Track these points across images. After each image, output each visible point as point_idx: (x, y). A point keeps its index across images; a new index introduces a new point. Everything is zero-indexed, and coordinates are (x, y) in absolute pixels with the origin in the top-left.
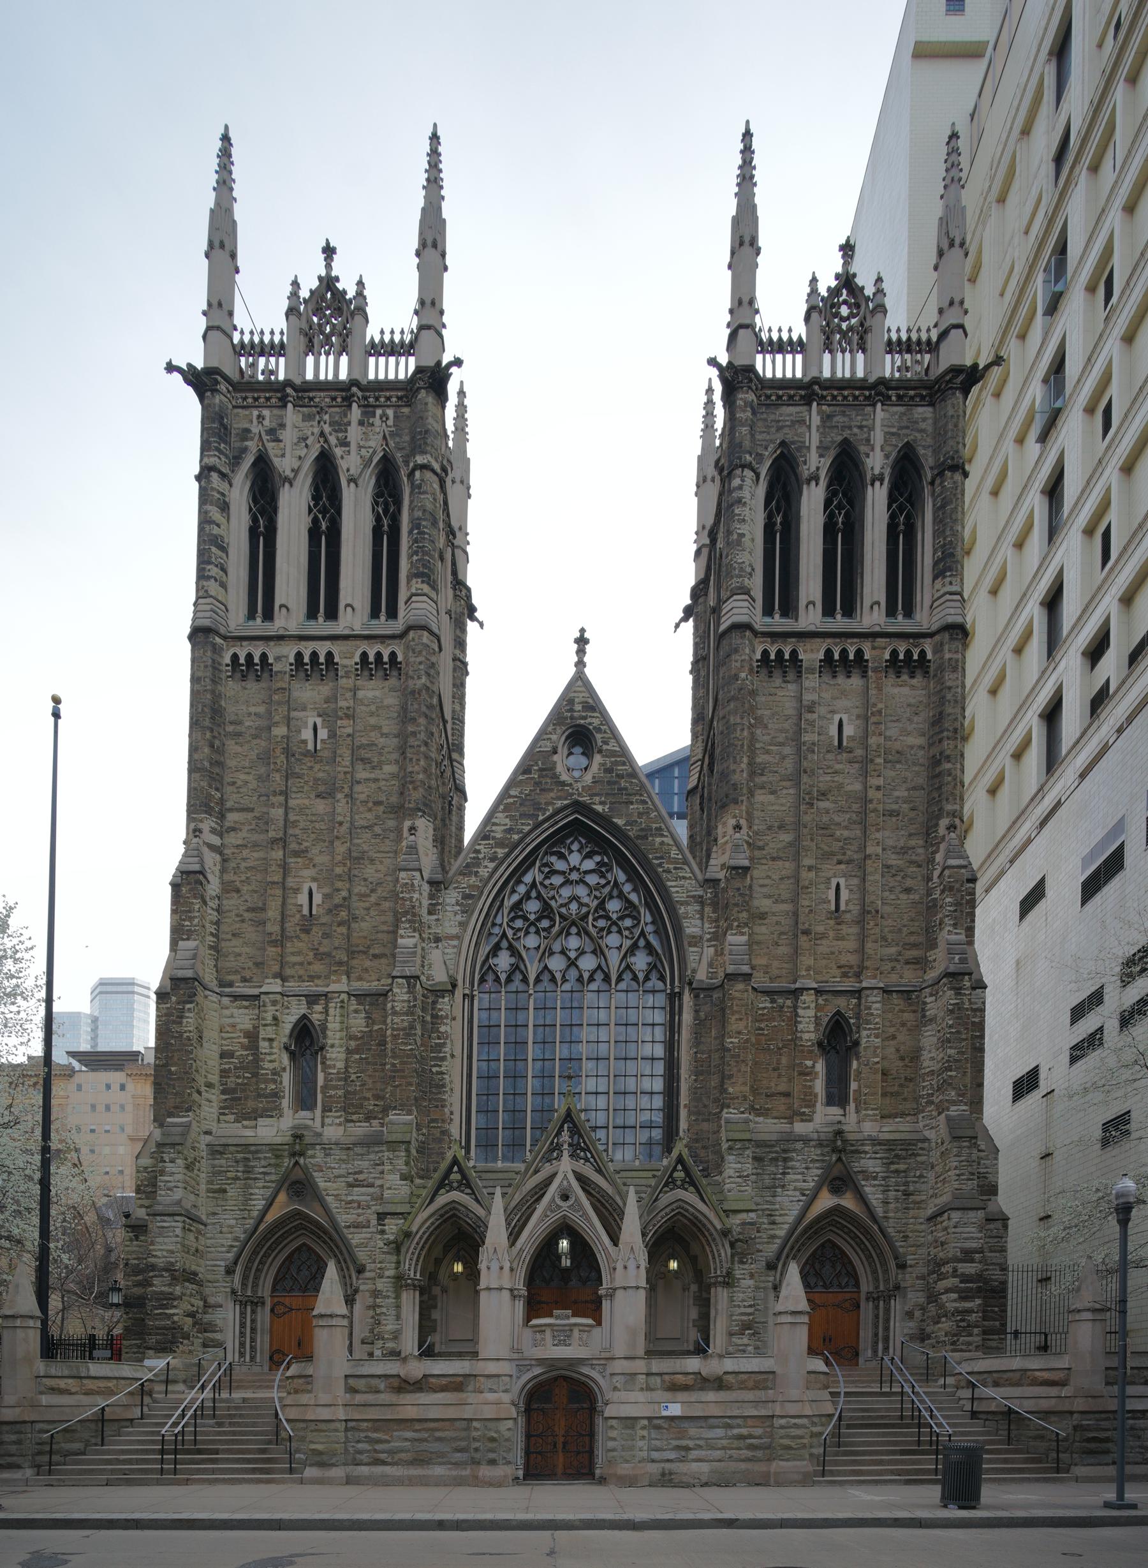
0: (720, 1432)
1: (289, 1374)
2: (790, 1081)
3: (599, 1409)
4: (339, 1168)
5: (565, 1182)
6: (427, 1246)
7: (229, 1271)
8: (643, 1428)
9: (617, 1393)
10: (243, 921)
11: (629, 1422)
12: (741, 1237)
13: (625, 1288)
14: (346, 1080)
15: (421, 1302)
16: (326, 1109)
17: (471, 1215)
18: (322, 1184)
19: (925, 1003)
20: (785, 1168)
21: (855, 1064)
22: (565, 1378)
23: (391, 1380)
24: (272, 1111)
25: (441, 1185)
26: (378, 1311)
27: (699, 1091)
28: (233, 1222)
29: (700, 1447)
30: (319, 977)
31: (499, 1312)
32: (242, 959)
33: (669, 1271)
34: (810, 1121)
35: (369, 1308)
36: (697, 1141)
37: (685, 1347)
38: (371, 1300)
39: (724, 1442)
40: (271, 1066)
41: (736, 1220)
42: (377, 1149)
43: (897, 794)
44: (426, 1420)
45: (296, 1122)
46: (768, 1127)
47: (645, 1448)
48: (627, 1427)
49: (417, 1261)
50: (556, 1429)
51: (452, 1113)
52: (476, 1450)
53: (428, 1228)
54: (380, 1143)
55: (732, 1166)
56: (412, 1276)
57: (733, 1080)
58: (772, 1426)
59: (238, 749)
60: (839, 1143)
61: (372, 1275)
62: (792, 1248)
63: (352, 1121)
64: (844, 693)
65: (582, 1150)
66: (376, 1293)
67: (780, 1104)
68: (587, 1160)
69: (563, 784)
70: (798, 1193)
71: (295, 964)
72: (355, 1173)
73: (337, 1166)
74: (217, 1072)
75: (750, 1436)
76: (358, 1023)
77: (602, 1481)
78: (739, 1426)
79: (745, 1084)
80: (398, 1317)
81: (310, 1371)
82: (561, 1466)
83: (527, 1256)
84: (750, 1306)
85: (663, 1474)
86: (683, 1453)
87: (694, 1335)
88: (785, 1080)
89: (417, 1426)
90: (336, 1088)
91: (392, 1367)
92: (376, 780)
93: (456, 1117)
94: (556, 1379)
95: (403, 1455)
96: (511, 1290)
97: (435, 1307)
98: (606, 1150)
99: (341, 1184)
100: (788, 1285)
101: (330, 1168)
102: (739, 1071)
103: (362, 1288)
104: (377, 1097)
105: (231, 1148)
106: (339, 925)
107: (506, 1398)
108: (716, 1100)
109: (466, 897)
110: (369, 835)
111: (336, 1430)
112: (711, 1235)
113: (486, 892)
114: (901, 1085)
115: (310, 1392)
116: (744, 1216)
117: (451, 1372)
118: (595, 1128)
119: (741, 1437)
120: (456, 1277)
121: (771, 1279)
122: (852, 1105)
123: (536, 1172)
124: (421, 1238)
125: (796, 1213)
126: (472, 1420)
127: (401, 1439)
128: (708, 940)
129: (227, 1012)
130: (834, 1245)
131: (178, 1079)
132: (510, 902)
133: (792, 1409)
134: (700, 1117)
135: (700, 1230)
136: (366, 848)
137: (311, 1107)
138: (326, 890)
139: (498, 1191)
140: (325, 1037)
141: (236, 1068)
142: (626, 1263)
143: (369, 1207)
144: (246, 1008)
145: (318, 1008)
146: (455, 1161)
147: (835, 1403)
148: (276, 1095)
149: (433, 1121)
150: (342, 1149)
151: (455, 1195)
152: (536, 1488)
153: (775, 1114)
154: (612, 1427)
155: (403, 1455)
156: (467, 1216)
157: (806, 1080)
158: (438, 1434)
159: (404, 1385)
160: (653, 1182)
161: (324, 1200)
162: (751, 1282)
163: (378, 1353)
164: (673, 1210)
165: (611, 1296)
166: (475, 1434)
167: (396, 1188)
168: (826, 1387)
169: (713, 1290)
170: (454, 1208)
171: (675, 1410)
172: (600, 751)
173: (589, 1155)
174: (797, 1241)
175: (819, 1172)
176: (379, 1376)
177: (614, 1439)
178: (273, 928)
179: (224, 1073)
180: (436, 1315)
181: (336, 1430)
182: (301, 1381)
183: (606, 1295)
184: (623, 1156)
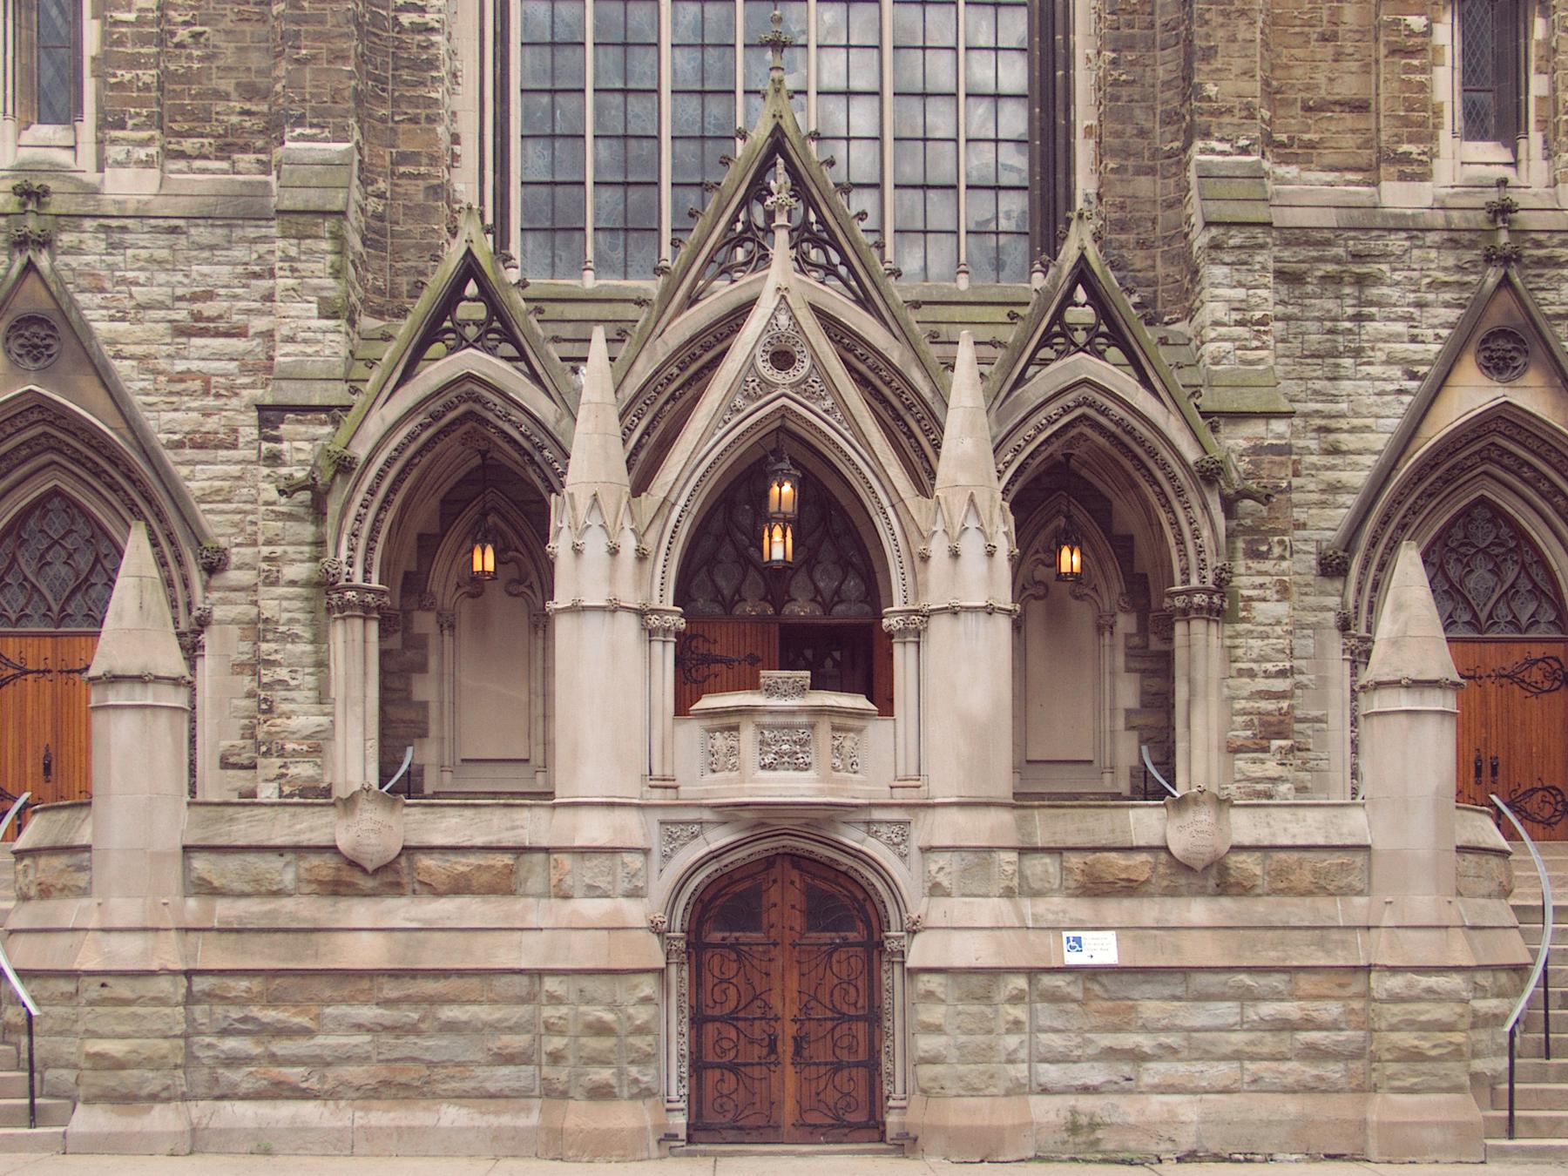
0: (1226, 1011)
1: (23, 842)
2: (1366, 70)
3: (890, 945)
4: (150, 282)
5: (783, 319)
6: (398, 499)
8: (1016, 999)
9: (941, 903)
11: (975, 980)
12: (1252, 484)
13: (954, 611)
14: (161, 42)
15: (384, 654)
16: (109, 122)
17: (517, 415)
18: (102, 328)
20: (1362, 303)
21: (1539, 28)
22: (798, 860)
23: (315, 860)
25: (432, 333)
26: (267, 675)
27: (1125, 92)
29: (1171, 1052)
31: (606, 668)
33: (1060, 577)
34: (1424, 177)
35: (239, 668)
36: (1122, 226)
37: (1107, 784)
38: (246, 646)
39: (1238, 1039)
41: (1235, 440)
42: (251, 232)
44: (414, 974)
45: (25, 154)
46: (1309, 194)
47: (1023, 1054)
48: (973, 997)
49: (372, 538)
50: (776, 1002)
51: (456, 139)
52: (556, 1058)
53: (400, 449)
54: (261, 217)
55: (1220, 290)
56: (358, 580)
57: (1218, 63)
58: (1367, 995)
60: (1503, 238)
61: (247, 577)
62: (1385, 521)
65: (818, 243)
66: (259, 628)
67: (1342, 131)
68: (830, 270)
70: (1396, 372)
72: (194, 298)
73: (142, 277)
75: (1309, 1024)
77: (906, 1145)
78: (1279, 997)
79: (1248, 73)
80: (322, 696)
81: (84, 836)
82: (789, 1106)
83: (681, 519)
84: (1282, 673)
85: (1074, 1128)
86: (1127, 1069)
87: (1128, 751)
88: (1354, 66)
89: (390, 990)
90: (134, 62)
91: (313, 826)
93: (468, 150)
94: (769, 861)
95: (353, 1073)
96: (642, 613)
97: (422, 668)
98: (880, 246)
99: (154, 326)
100: (1399, 607)
101: (123, 281)
102: (1232, 39)
103: (217, 613)
104: (250, 91)
107: (636, 912)
108: (1170, 118)
111: (160, 1001)
112: (1172, 478)
115: (84, 892)
116: (1257, 428)
117: (479, 841)
118: (846, 188)
119: (1284, 1026)
120: (477, 584)
121: (1334, 601)
122: (1535, 138)
123: (692, 300)
124: (380, 476)
125: (1393, 424)
126: (540, 973)
127: (343, 1029)
130: (1498, 515)
133: (1422, 949)
134: (1131, 163)
135: (1141, 465)
137: (69, 114)
139: (598, 348)
142: (954, 550)
143: (233, 391)
146: (470, 268)
147: (1530, 937)
149: (404, 158)
150: (155, 230)
151: (472, 360)
152: (724, 1162)
153: (1330, 158)
154: (929, 995)
155: (353, 1073)
156: (506, 417)
157: (1409, 69)
158: (449, 1013)
159: (350, 876)
160: (1009, 334)
161: (107, 367)
162: (1281, 609)
163: (268, 792)
164: (1066, 410)
165: (918, 636)
166: (549, 1012)
167: (311, 341)
168: (1506, 893)
169: (1180, 628)
170: (478, 399)
171: (1101, 949)
173: (835, 258)
174: (1397, 501)
175: (1453, 315)
176: (279, 850)
177: (937, 1029)
180: (425, 689)
181: (160, 1001)
182: (60, 862)
183: (904, 632)
184: (916, 267)
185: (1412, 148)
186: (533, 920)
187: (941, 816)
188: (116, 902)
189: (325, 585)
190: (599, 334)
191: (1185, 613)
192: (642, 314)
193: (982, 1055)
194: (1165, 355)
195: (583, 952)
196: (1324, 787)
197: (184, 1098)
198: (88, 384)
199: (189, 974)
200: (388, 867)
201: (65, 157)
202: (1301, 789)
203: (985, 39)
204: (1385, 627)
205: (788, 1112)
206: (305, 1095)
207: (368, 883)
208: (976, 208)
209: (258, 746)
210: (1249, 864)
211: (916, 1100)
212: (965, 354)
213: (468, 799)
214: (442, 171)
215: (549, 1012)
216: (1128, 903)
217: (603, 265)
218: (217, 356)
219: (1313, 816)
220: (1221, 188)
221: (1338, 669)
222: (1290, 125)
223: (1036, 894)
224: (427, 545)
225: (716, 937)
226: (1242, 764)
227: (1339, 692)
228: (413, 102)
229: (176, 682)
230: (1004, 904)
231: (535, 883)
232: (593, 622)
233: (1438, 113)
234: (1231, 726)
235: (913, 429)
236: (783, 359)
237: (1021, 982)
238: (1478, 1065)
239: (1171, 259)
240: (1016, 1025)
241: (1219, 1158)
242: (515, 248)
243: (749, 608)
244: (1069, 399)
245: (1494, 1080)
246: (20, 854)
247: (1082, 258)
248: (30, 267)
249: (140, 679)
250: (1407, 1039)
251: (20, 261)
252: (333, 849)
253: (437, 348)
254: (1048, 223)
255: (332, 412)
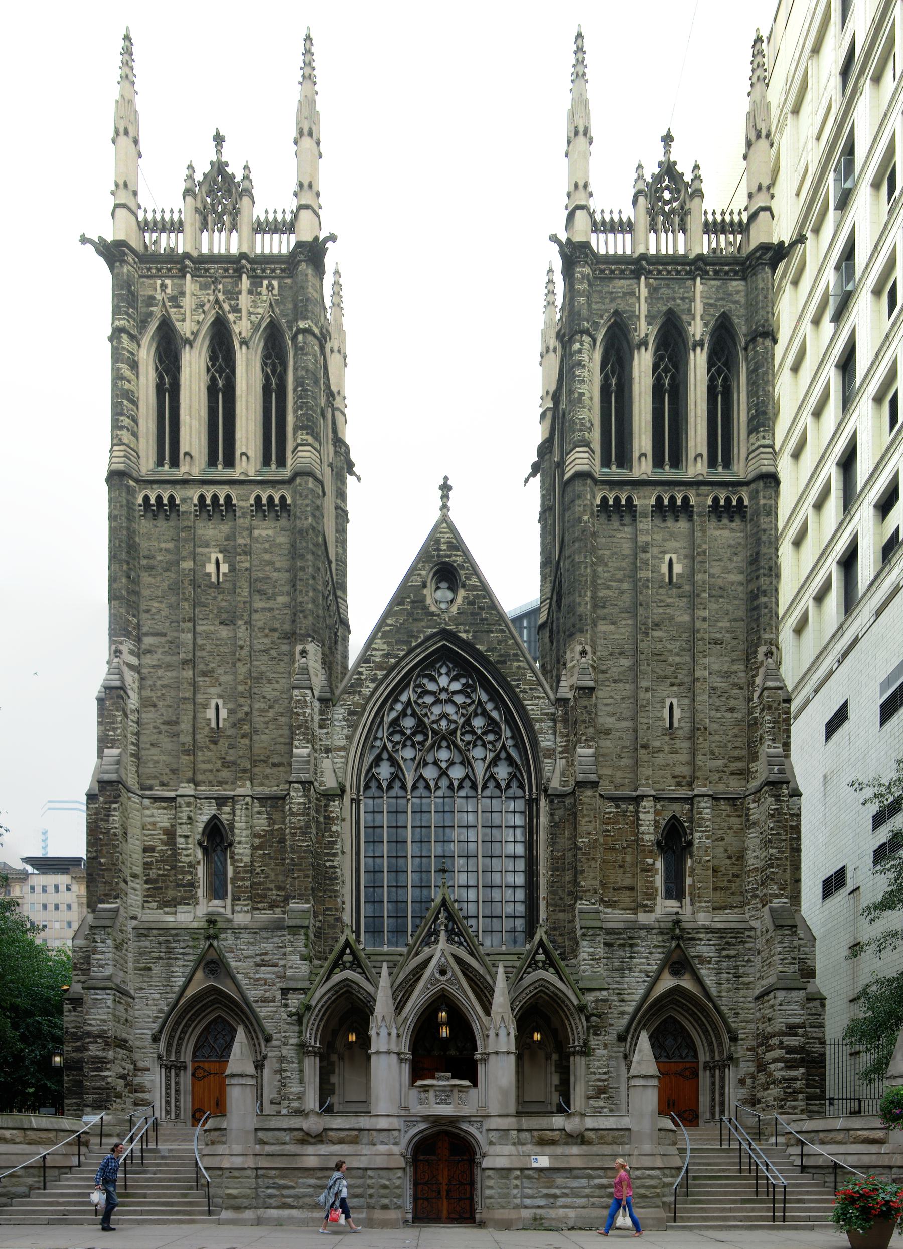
0: (584, 1182)
1: (206, 1127)
5: (443, 959)
7: (155, 1039)
8: (517, 1178)
9: (493, 1147)
10: (160, 733)
13: (497, 1053)
14: (252, 873)
15: (321, 1068)
16: (236, 898)
17: (362, 991)
18: (233, 964)
19: (749, 809)
21: (689, 863)
22: (447, 1133)
23: (296, 1133)
24: (189, 899)
26: (284, 1074)
28: (157, 996)
29: (566, 1195)
30: (226, 783)
31: (387, 1072)
32: (160, 765)
34: (652, 912)
35: (276, 1072)
36: (555, 929)
37: (549, 1109)
39: (588, 1191)
40: (187, 860)
41: (590, 997)
43: (720, 624)
46: (615, 917)
49: (317, 1031)
51: (343, 903)
52: (371, 1196)
53: (326, 1002)
54: (282, 928)
55: (586, 950)
59: (150, 580)
60: (677, 931)
62: (638, 1024)
63: (258, 909)
64: (673, 535)
65: (456, 934)
66: (282, 1059)
67: (625, 897)
68: (460, 944)
69: (433, 614)
70: (643, 975)
71: (205, 771)
72: (262, 954)
74: (141, 864)
76: (261, 823)
77: (482, 1225)
78: (600, 1177)
79: (595, 878)
80: (301, 1081)
84: (605, 1073)
85: (535, 1219)
86: (552, 1201)
87: (556, 1098)
90: (243, 879)
91: (296, 1122)
92: (271, 610)
93: (347, 906)
96: (398, 1054)
97: (333, 1072)
98: (477, 936)
99: (250, 963)
100: (640, 1051)
103: (269, 1055)
104: (279, 888)
105: (155, 931)
106: (243, 736)
107: (396, 1150)
109: (351, 713)
110: (266, 658)
111: (248, 1177)
113: (368, 709)
114: (729, 881)
115: (224, 1143)
116: (597, 994)
118: (466, 917)
121: (622, 1049)
122: (688, 898)
123: (417, 954)
126: (366, 1169)
128: (561, 752)
129: (148, 812)
131: (107, 870)
132: (388, 719)
133: (647, 1162)
135: (566, 1015)
136: (263, 668)
138: (231, 706)
139: (385, 971)
140: (233, 835)
141: (157, 861)
142: (498, 1033)
143: (274, 984)
144: (165, 808)
145: (227, 809)
146: (347, 944)
147: (683, 1158)
148: (192, 885)
149: (327, 909)
151: (348, 974)
153: (622, 906)
154: (489, 1177)
155: (307, 1200)
157: (647, 876)
159: (308, 1138)
160: (517, 964)
162: (604, 1052)
163: (284, 1112)
165: (485, 1061)
166: (369, 1182)
167: (297, 967)
168: (675, 1144)
169: (572, 1059)
171: (543, 1162)
172: (463, 586)
174: (643, 1017)
175: (661, 956)
177: (491, 1188)
178: (186, 739)
179: (147, 866)
180: (334, 1079)
181: (248, 1177)
182: (217, 1133)
184: (488, 943)
185: (648, 902)
186: (364, 1152)
187: (492, 1119)
188: (234, 1146)
189: (302, 1046)
190: (385, 965)
191: (574, 1054)
192: (401, 959)
193: (506, 1196)
194: (567, 970)
195: (380, 1162)
196: (619, 1110)
197: (255, 1208)
198: (229, 982)
199: (257, 1169)
200: (319, 1135)
201: (222, 910)
202: (611, 1110)
203: (511, 868)
204: (636, 1058)
205: (445, 1214)
206: (293, 1207)
207: (312, 1140)
208: (508, 924)
209: (282, 1097)
210: (591, 1134)
211: (485, 1210)
212: (501, 970)
213: (343, 1113)
214: (339, 913)
215: (369, 1182)
216: (552, 1147)
217: (390, 943)
218: (269, 973)
219: (612, 1119)
220: (586, 916)
221: (623, 1070)
222: (609, 895)
223: (523, 1144)
224: (335, 1033)
225: (422, 1157)
226: (592, 1102)
227: (623, 1079)
228: (330, 891)
229: (252, 1076)
230: (513, 1148)
231: (365, 1140)
232: (383, 1057)
233: (656, 890)
234: (588, 1090)
235: (484, 993)
236: (443, 972)
237: (518, 1173)
238: (665, 1199)
239: (570, 939)
240: (516, 1187)
241: (581, 1229)
242: (362, 938)
243: (436, 1053)
244: (537, 985)
245: (670, 1204)
246: (206, 1131)
247: (541, 939)
248: (211, 945)
249: (241, 1075)
250: (642, 1191)
251: (208, 943)
252: (301, 1129)
253: (337, 970)
254: (530, 932)
255: (304, 991)
